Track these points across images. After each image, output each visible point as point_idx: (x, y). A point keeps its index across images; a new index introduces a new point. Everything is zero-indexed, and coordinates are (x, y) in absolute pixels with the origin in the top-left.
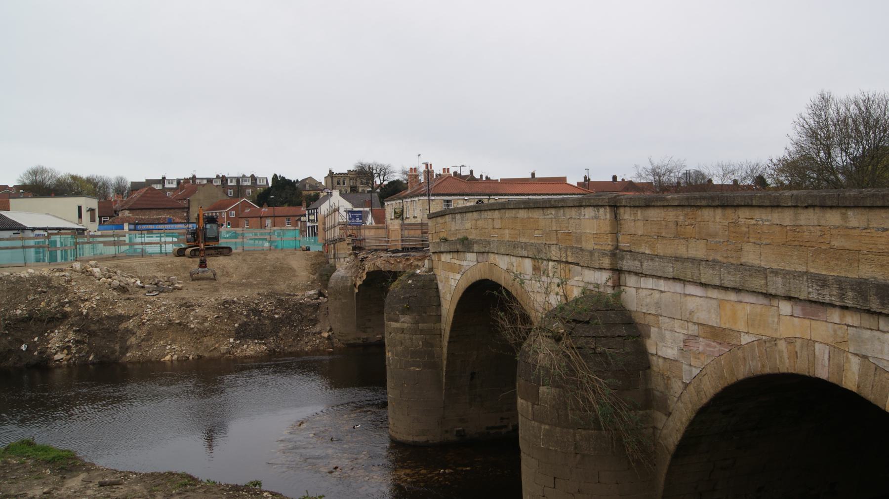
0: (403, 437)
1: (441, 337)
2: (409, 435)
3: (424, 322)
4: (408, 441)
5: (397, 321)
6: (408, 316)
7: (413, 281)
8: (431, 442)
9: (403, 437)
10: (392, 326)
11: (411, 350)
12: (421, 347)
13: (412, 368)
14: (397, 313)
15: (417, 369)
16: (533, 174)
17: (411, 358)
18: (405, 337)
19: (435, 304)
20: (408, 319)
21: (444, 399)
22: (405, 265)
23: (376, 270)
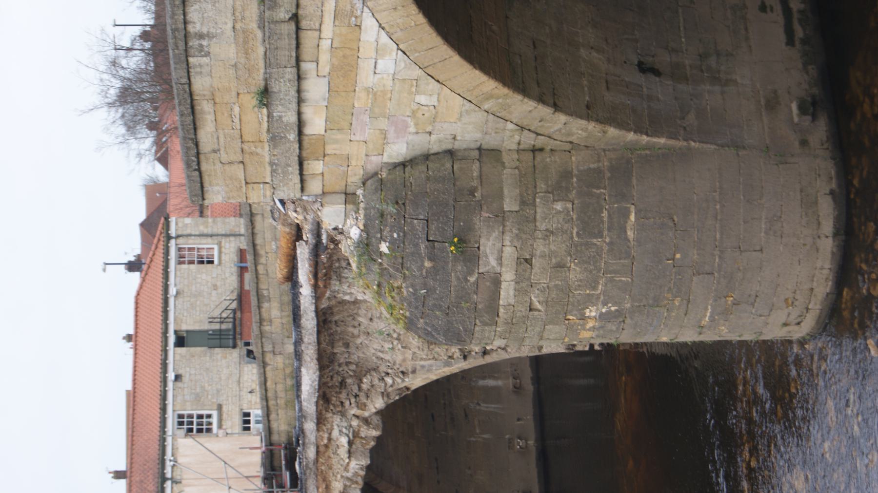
0: (822, 268)
1: (541, 150)
2: (817, 250)
3: (500, 196)
4: (833, 253)
5: (496, 281)
6: (482, 241)
7: (382, 239)
8: (834, 185)
9: (822, 268)
10: (512, 301)
11: (578, 234)
12: (569, 205)
13: (630, 234)
14: (472, 279)
15: (632, 217)
16: (118, 475)
17: (600, 235)
18: (543, 256)
19: (448, 165)
20: (490, 243)
21: (713, 147)
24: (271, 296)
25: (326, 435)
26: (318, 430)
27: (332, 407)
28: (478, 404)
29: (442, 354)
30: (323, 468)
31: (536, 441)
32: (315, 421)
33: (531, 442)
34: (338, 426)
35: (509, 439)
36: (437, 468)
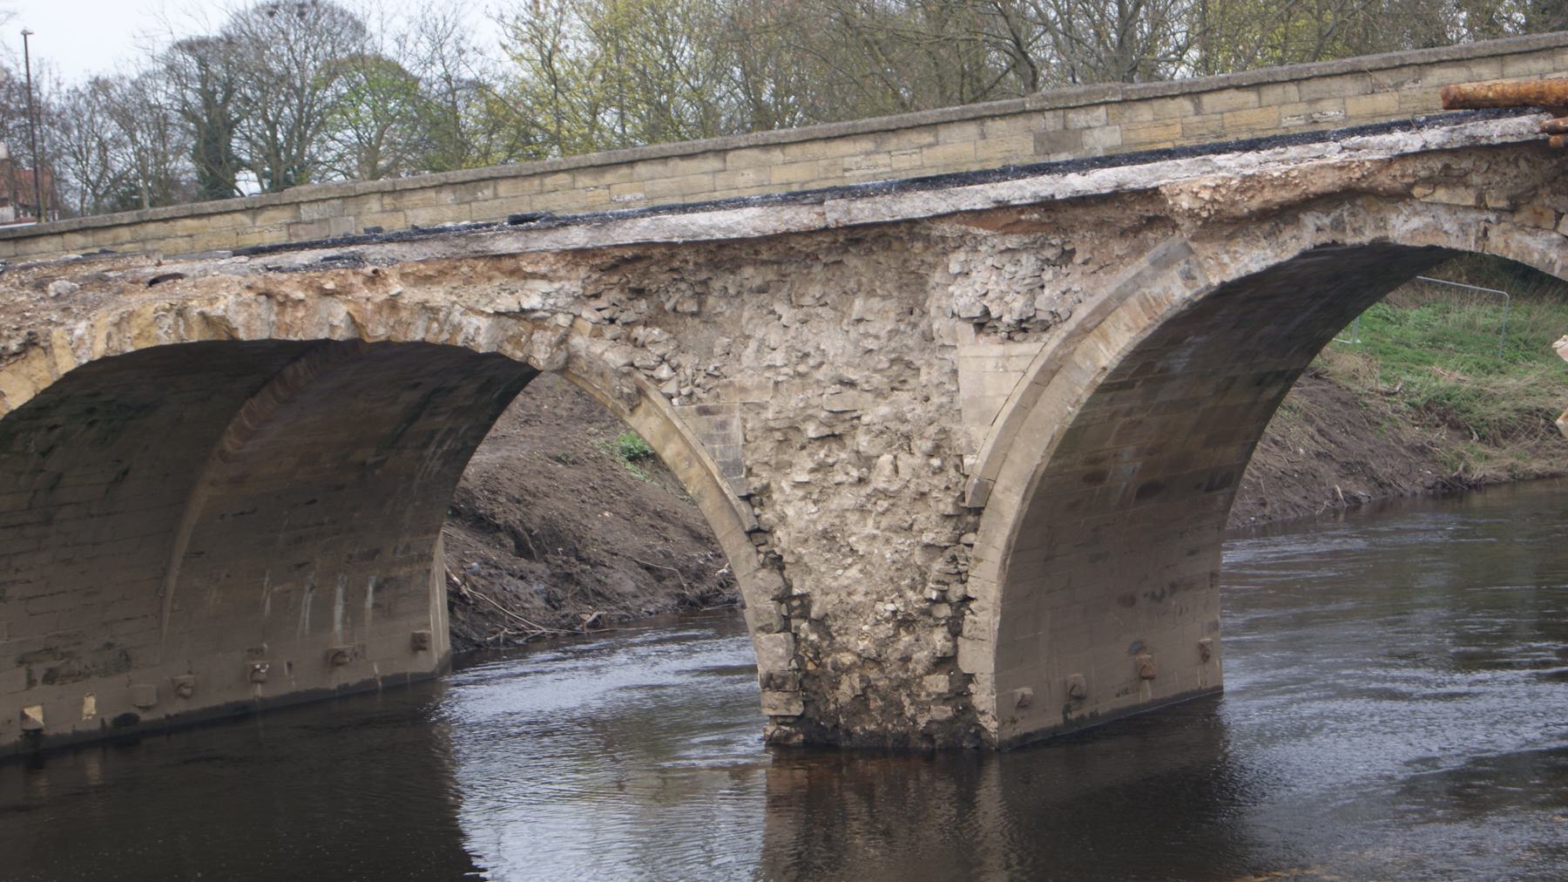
22: (370, 306)
23: (195, 337)
24: (473, 204)
25: (543, 269)
26: (563, 253)
27: (595, 276)
28: (312, 588)
29: (756, 456)
30: (465, 269)
31: (263, 700)
32: (589, 246)
33: (259, 691)
34: (557, 291)
35: (262, 650)
36: (242, 513)
